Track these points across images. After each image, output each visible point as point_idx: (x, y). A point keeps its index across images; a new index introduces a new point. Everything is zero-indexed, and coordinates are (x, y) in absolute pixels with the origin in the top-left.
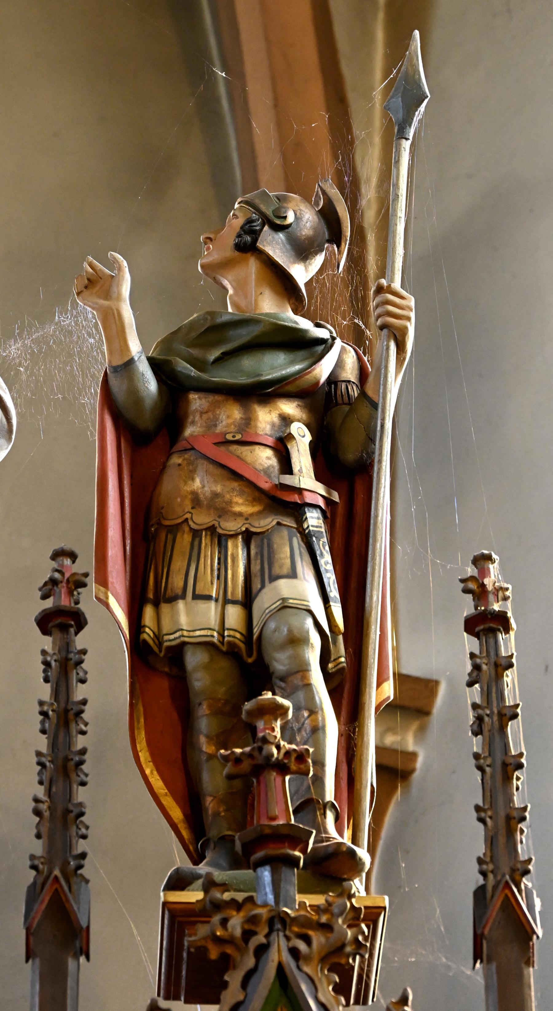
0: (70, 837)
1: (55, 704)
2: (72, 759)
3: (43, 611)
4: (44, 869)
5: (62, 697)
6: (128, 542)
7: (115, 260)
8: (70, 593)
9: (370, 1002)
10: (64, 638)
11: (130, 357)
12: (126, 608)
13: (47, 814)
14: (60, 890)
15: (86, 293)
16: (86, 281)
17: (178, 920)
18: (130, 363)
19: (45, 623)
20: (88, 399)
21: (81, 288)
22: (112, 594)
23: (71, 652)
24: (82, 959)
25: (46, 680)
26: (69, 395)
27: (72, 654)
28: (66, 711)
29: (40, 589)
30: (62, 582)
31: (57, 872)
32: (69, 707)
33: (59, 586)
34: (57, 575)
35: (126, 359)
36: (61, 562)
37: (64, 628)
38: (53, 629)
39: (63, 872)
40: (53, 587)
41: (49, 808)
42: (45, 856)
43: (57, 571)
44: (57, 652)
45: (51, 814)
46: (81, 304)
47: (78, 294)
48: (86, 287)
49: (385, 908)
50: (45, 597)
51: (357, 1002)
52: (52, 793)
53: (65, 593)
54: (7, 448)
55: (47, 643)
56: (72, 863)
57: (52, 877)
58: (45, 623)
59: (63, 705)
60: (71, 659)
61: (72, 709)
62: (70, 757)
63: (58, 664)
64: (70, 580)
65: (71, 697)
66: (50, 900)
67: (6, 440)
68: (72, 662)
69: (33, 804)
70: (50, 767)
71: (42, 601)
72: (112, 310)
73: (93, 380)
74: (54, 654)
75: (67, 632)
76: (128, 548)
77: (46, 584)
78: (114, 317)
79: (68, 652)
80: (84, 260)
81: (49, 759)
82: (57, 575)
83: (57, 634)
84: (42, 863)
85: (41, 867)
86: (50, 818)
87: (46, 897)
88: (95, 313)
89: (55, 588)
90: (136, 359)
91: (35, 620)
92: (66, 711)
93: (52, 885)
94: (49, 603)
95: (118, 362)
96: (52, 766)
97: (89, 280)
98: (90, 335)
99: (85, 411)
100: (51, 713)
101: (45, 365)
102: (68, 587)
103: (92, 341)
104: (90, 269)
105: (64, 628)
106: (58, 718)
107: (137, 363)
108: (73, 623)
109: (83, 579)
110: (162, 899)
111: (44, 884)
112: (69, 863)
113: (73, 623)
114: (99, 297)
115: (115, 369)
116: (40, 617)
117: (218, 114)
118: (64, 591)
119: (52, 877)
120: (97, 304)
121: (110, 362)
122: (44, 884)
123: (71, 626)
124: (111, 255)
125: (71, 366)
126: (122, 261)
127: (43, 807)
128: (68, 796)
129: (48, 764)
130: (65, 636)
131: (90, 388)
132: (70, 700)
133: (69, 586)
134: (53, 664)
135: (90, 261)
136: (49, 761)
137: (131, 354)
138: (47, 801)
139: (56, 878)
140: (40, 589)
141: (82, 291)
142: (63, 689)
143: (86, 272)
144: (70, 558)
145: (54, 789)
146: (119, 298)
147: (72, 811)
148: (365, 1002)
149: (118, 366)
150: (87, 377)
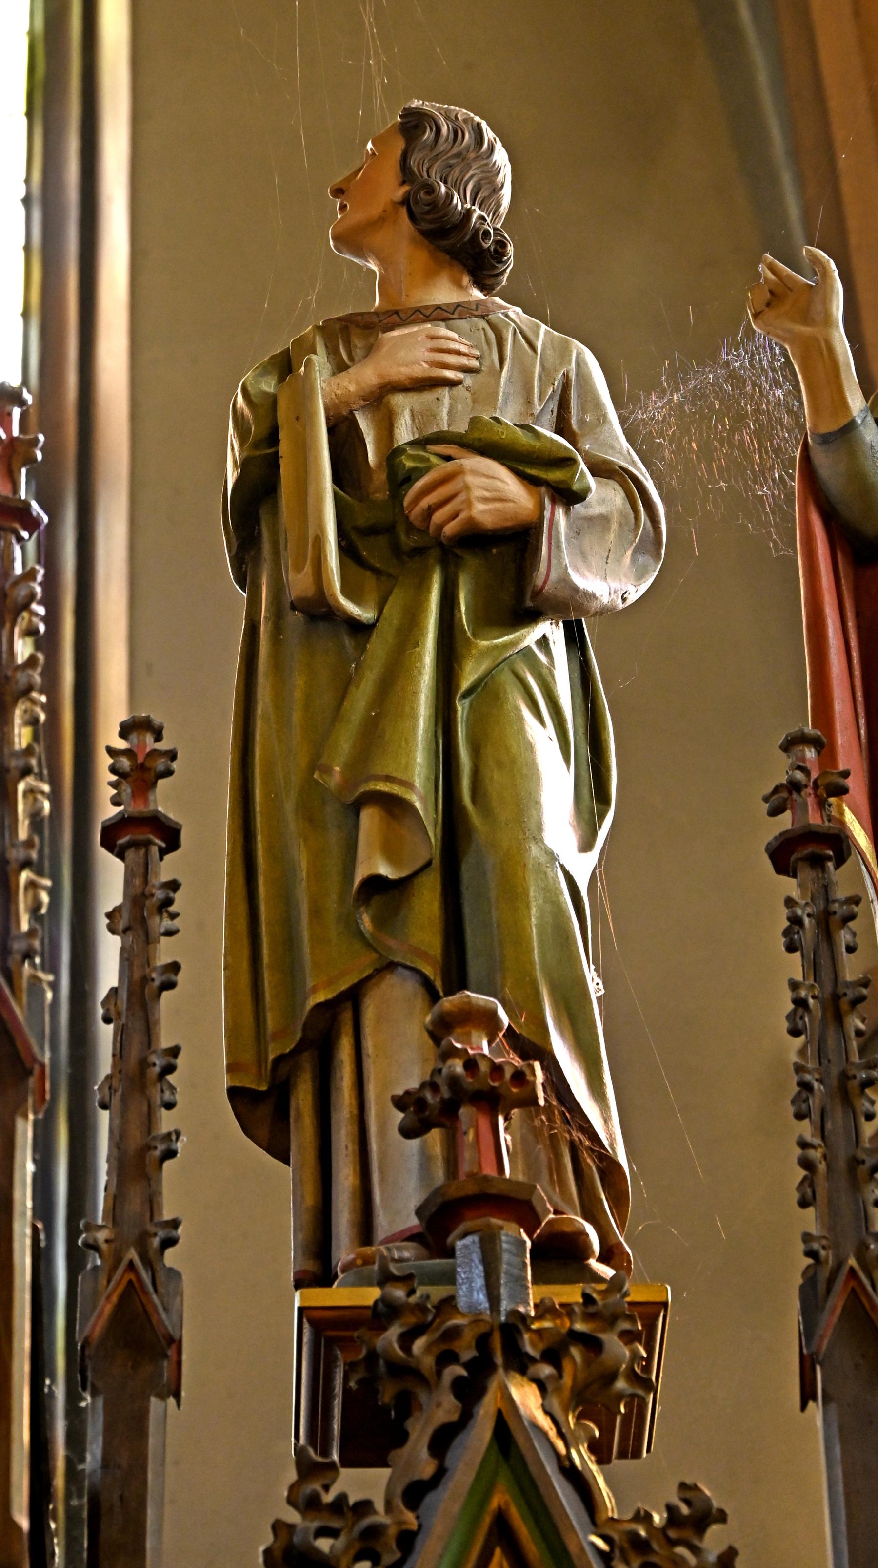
0: (864, 1202)
1: (816, 985)
2: (855, 1077)
3: (782, 834)
4: (827, 1257)
5: (826, 975)
6: (862, 721)
7: (815, 260)
8: (822, 804)
9: (645, 1454)
10: (818, 878)
11: (850, 419)
12: (869, 826)
13: (822, 1167)
14: (858, 1290)
15: (770, 315)
16: (768, 295)
17: (328, 1333)
18: (850, 427)
19: (784, 855)
20: (769, 489)
21: (760, 306)
22: (849, 808)
23: (834, 901)
24: (171, 1401)
25: (791, 948)
26: (737, 481)
27: (837, 905)
28: (836, 998)
29: (766, 799)
30: (806, 786)
31: (852, 1262)
32: (841, 990)
33: (803, 793)
34: (799, 775)
35: (843, 422)
36: (800, 754)
37: (817, 862)
38: (800, 865)
39: (860, 1259)
40: (790, 793)
41: (825, 1157)
42: (825, 1234)
43: (799, 768)
44: (809, 901)
45: (828, 1166)
46: (760, 331)
47: (756, 315)
48: (768, 305)
49: (665, 1305)
50: (775, 812)
51: (622, 1455)
52: (826, 1133)
53: (812, 806)
54: (654, 571)
55: (790, 886)
56: (872, 1246)
57: (845, 1270)
58: (784, 855)
59: (829, 989)
60: (835, 913)
61: (845, 994)
62: (851, 1073)
63: (813, 921)
64: (820, 782)
65: (841, 975)
66: (844, 1308)
67: (651, 556)
68: (837, 917)
69: (798, 1151)
70: (819, 1090)
71: (772, 818)
72: (817, 339)
73: (777, 457)
74: (807, 904)
75: (823, 869)
76: (862, 732)
77: (777, 790)
78: (822, 354)
79: (828, 901)
80: (759, 259)
81: (817, 1076)
82: (799, 775)
83: (807, 873)
84: (824, 1248)
85: (823, 1253)
86: (828, 1172)
87: (837, 1302)
88: (787, 347)
89: (795, 796)
90: (859, 421)
91: (767, 850)
92: (836, 998)
93: (846, 1282)
94: (785, 821)
95: (829, 426)
96: (822, 1088)
97: (771, 292)
98: (777, 384)
99: (765, 508)
100: (811, 1001)
101: (701, 433)
102: (816, 795)
103: (779, 393)
104: (770, 276)
105: (817, 862)
106: (824, 1009)
107: (862, 428)
108: (831, 853)
109: (841, 781)
110: (297, 1304)
111: (831, 1282)
112: (868, 1247)
113: (831, 853)
114: (793, 320)
115: (826, 439)
116: (775, 844)
117: (734, 30)
118: (811, 801)
119: (845, 1270)
120: (789, 331)
121: (815, 425)
122: (831, 1282)
123: (829, 858)
124: (808, 251)
125: (742, 436)
126: (828, 261)
127: (816, 1155)
128: (854, 1135)
129: (816, 1085)
130: (820, 875)
131: (772, 468)
132: (840, 980)
133: (819, 793)
134: (807, 921)
135: (768, 261)
136: (817, 1080)
137: (851, 414)
138: (820, 1146)
139: (852, 1269)
140: (766, 799)
141: (760, 312)
142: (825, 962)
143: (766, 279)
144: (815, 748)
145: (829, 1126)
146: (827, 321)
147: (863, 1162)
148: (637, 1454)
149: (830, 433)
150: (767, 453)
